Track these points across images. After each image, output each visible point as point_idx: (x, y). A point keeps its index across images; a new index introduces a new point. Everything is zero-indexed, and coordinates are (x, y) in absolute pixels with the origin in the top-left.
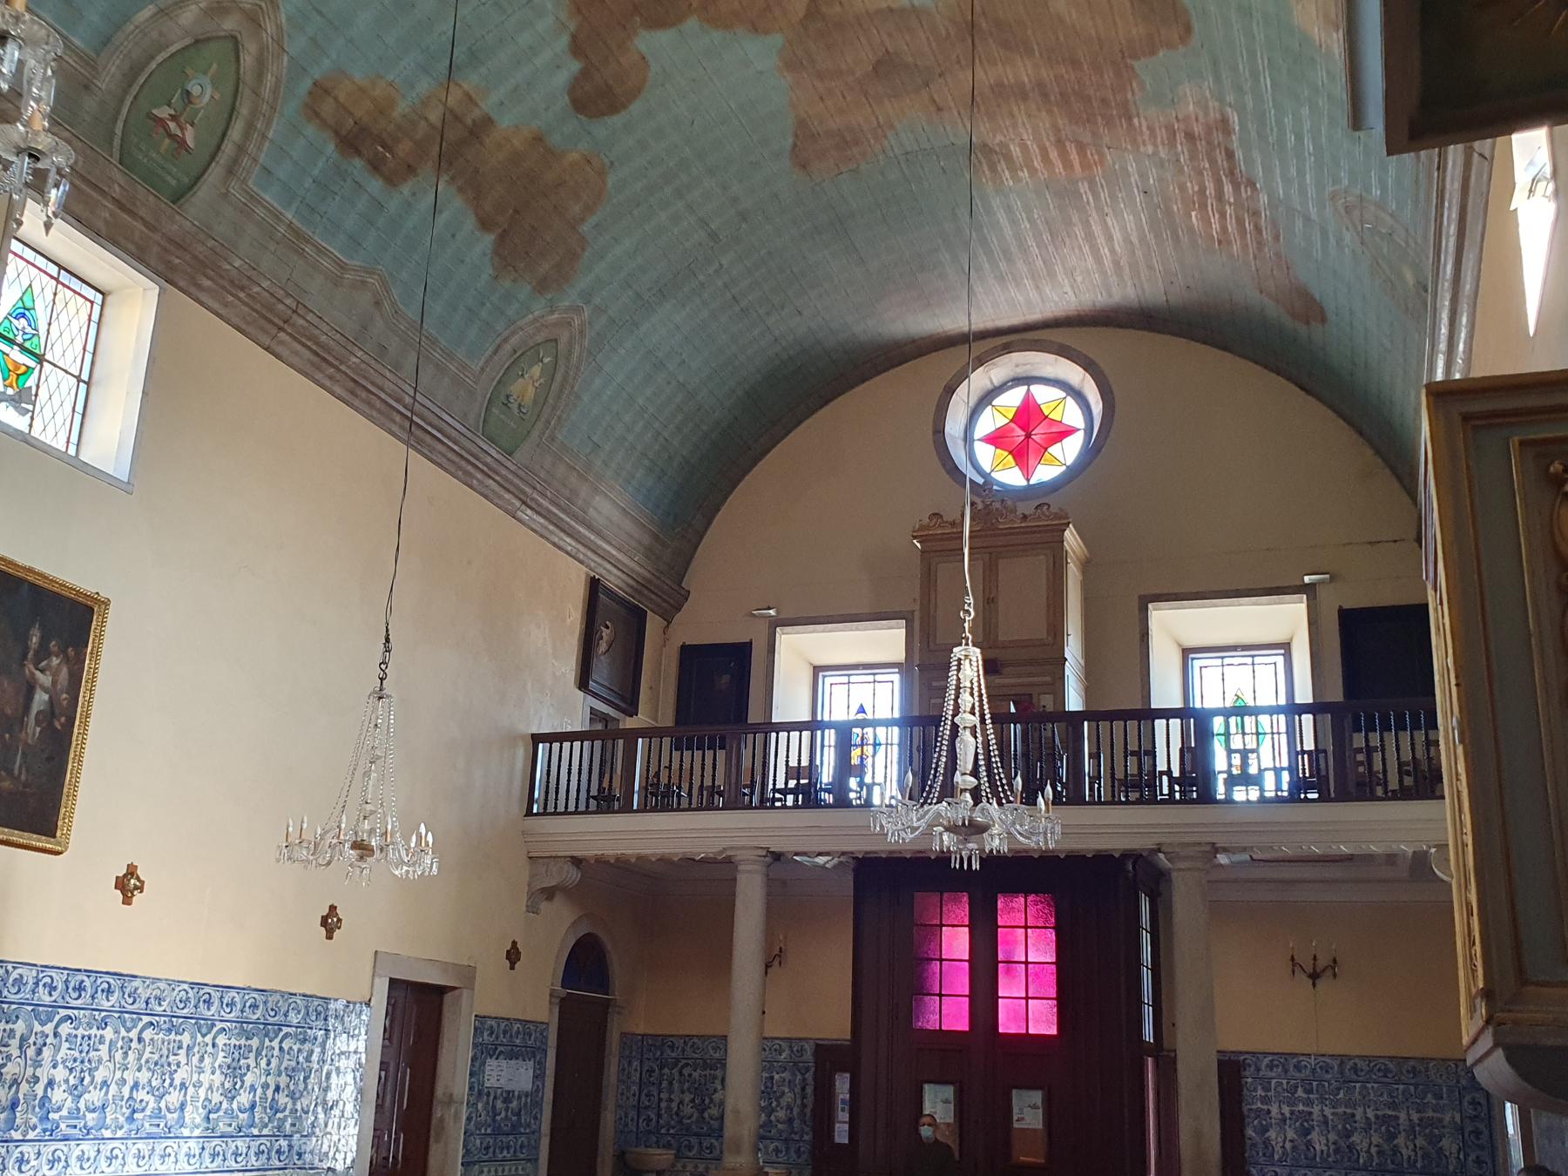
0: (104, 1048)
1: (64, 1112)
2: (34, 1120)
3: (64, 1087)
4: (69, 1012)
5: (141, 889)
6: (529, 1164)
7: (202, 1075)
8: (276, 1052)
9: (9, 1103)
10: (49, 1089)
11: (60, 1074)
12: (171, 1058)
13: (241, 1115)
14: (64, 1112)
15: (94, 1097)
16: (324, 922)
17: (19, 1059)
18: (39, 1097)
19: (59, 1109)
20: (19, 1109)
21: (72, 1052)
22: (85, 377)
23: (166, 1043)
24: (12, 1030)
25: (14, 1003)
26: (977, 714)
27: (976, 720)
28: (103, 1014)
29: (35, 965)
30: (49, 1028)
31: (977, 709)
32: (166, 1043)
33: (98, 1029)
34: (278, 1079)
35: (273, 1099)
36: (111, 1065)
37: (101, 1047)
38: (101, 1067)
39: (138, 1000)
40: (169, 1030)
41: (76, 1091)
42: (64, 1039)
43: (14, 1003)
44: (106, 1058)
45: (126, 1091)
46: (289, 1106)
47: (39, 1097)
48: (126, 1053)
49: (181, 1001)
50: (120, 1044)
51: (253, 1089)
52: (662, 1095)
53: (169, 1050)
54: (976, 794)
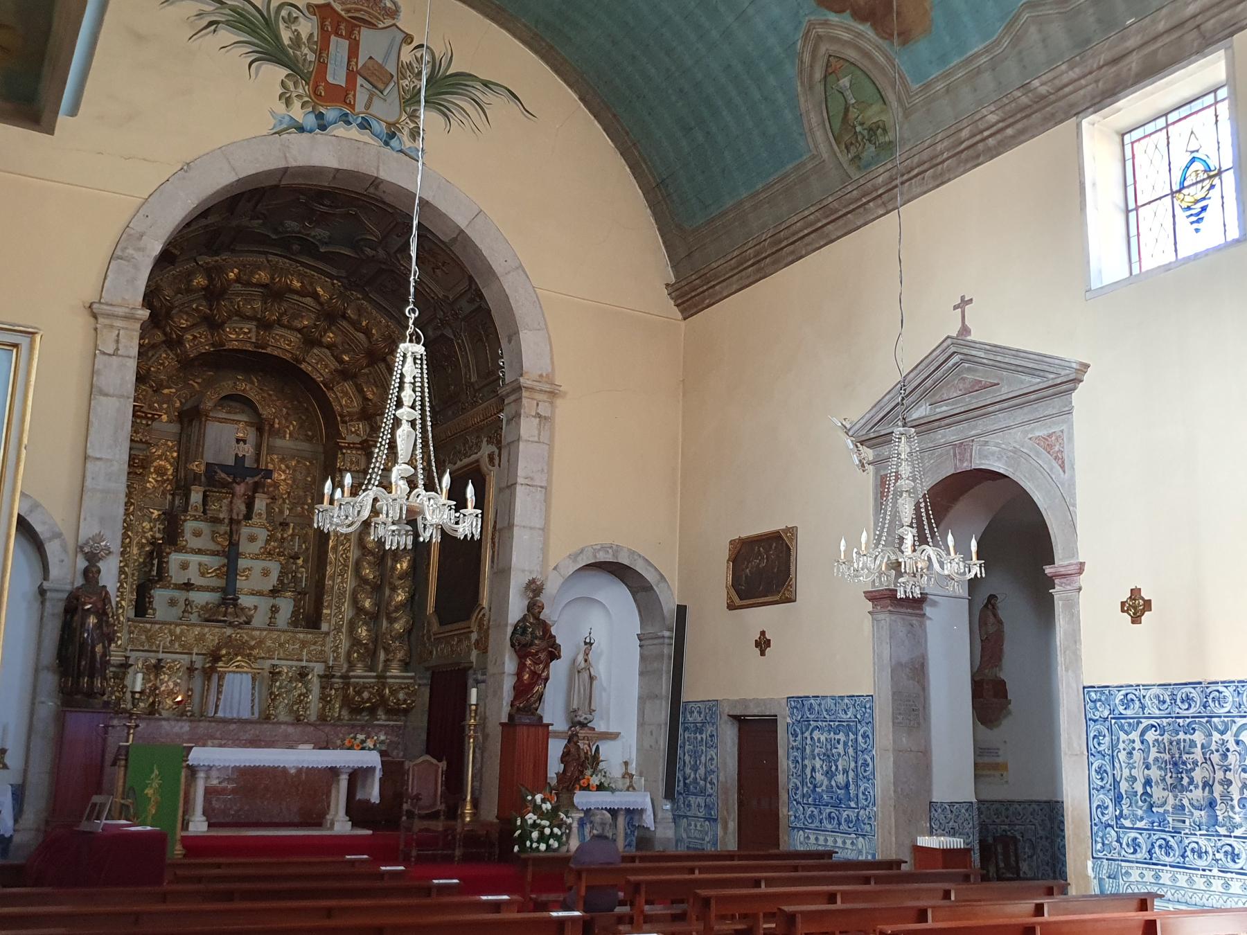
0: (840, 747)
1: (824, 787)
2: (1140, 812)
3: (1161, 786)
4: (1152, 722)
5: (1123, 604)
6: (707, 823)
7: (1228, 773)
8: (1138, 745)
9: (1208, 803)
10: (1148, 788)
11: (818, 763)
12: (834, 751)
13: (839, 791)
14: (824, 787)
15: (840, 778)
16: (768, 643)
17: (1204, 765)
18: (1139, 794)
19: (821, 786)
20: (1124, 802)
21: (1162, 755)
22: (1161, 122)
23: (1175, 743)
24: (1192, 741)
25: (1188, 717)
26: (418, 407)
27: (417, 414)
28: (1188, 720)
29: (1170, 685)
30: (1135, 735)
31: (418, 403)
32: (1175, 743)
33: (834, 733)
34: (813, 761)
35: (812, 776)
36: (847, 758)
37: (838, 746)
38: (840, 759)
39: (1193, 705)
40: (829, 731)
41: (829, 774)
42: (1151, 745)
43: (1188, 717)
44: (842, 753)
45: (1139, 788)
46: (692, 776)
47: (1139, 794)
48: (1130, 753)
49: (1132, 700)
50: (850, 743)
51: (845, 772)
52: (806, 762)
53: (1179, 749)
54: (412, 483)
